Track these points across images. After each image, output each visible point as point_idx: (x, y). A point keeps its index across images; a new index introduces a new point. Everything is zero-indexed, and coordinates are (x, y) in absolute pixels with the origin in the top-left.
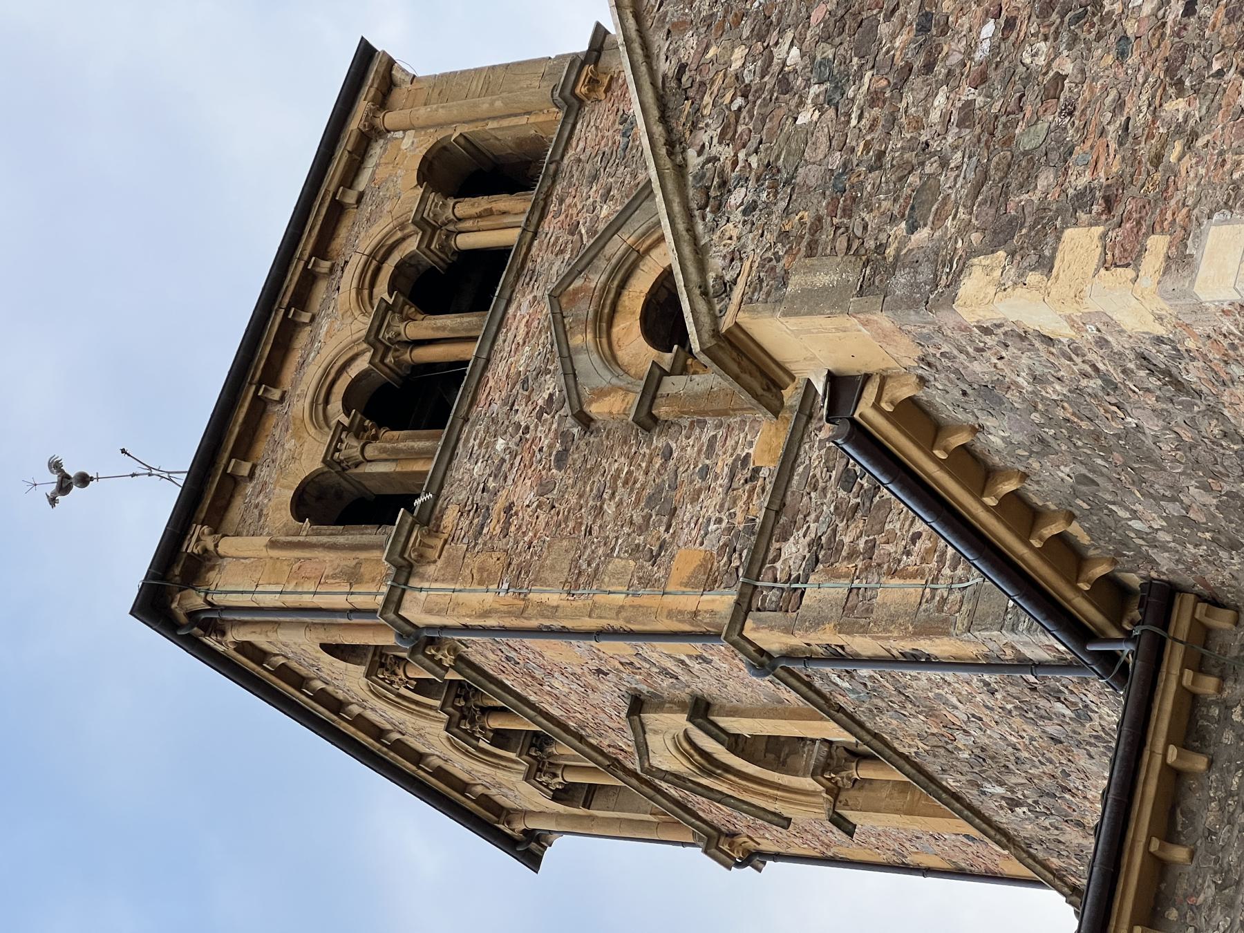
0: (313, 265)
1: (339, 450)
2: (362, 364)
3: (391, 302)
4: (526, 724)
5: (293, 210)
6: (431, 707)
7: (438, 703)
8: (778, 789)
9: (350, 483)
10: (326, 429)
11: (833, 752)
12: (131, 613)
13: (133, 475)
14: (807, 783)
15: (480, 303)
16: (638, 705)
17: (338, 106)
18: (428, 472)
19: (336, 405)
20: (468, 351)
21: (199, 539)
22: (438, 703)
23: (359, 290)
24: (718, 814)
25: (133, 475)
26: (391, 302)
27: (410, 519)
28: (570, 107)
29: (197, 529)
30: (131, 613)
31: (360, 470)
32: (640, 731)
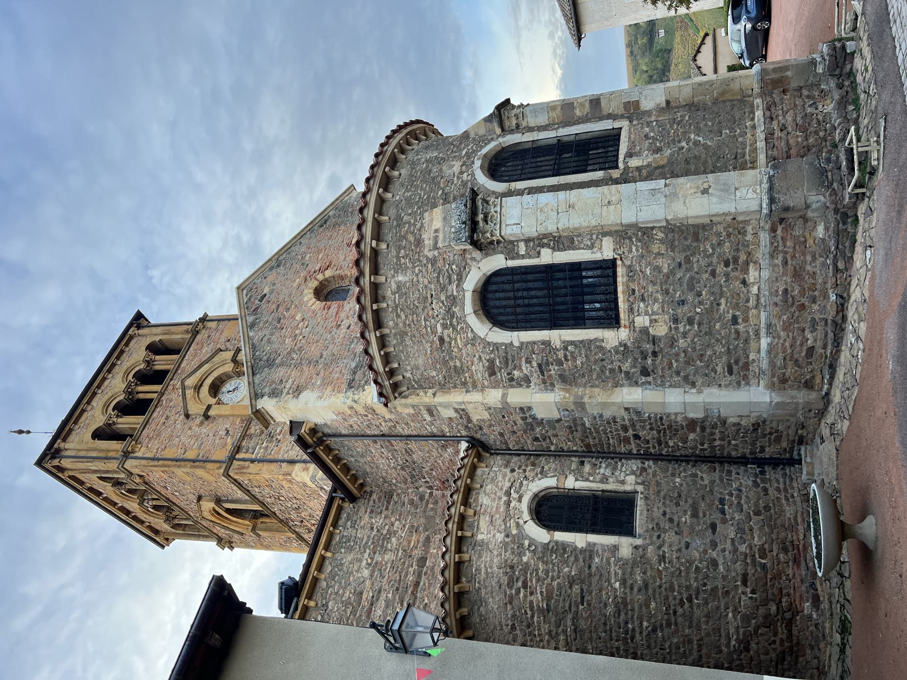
29: (59, 441)
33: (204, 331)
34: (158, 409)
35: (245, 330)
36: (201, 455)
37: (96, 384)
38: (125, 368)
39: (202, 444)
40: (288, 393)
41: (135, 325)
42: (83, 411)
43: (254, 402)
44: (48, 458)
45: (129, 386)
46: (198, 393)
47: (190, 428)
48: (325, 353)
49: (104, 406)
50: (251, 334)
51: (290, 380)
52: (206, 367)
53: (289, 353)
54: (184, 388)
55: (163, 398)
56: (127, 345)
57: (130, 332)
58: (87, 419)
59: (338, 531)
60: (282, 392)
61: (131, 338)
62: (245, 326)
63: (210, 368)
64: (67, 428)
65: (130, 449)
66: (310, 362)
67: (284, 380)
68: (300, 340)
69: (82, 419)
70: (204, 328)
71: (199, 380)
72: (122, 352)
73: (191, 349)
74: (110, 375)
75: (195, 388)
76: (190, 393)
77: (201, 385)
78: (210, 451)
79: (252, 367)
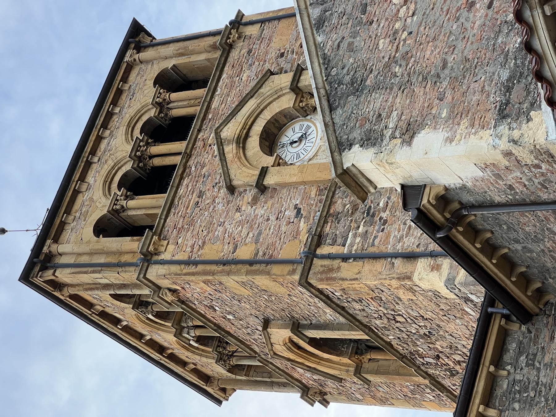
0: (101, 133)
1: (116, 205)
2: (128, 167)
3: (141, 138)
4: (210, 332)
5: (56, 193)
6: (208, 352)
7: (170, 325)
8: (189, 308)
9: (553, 78)
10: (108, 196)
11: (359, 346)
12: (19, 280)
13: (27, 231)
14: (346, 360)
15: (182, 137)
16: (266, 323)
17: (114, 66)
18: (158, 213)
19: (115, 185)
20: (177, 160)
21: (49, 246)
22: (170, 325)
23: (126, 133)
24: (307, 377)
25: (27, 231)
26: (141, 138)
27: (151, 234)
28: (224, 49)
29: (49, 242)
30: (19, 280)
31: (125, 214)
32: (268, 337)
33: (240, 44)
34: (185, 182)
35: (309, 33)
36: (261, 253)
37: (88, 148)
38: (127, 118)
39: (260, 234)
40: (393, 137)
41: (133, 46)
42: (76, 193)
43: (337, 157)
44: (37, 269)
45: (136, 148)
46: (244, 149)
47: (238, 210)
48: (450, 59)
49: (105, 182)
50: (319, 39)
51: (395, 113)
52: (251, 105)
53: (387, 66)
54: (220, 143)
55: (191, 163)
56: (125, 79)
57: (127, 58)
58: (83, 205)
59: (505, 373)
60: (382, 135)
61: (130, 67)
62: (307, 26)
63: (258, 106)
64: (57, 221)
65: (151, 248)
66: (425, 79)
67: (384, 115)
68: (405, 40)
69: (80, 200)
70: (239, 37)
71: (243, 128)
72: (119, 92)
73: (224, 76)
74: (107, 132)
75: (238, 142)
76: (230, 150)
77: (247, 136)
78: (273, 244)
79: (328, 96)
